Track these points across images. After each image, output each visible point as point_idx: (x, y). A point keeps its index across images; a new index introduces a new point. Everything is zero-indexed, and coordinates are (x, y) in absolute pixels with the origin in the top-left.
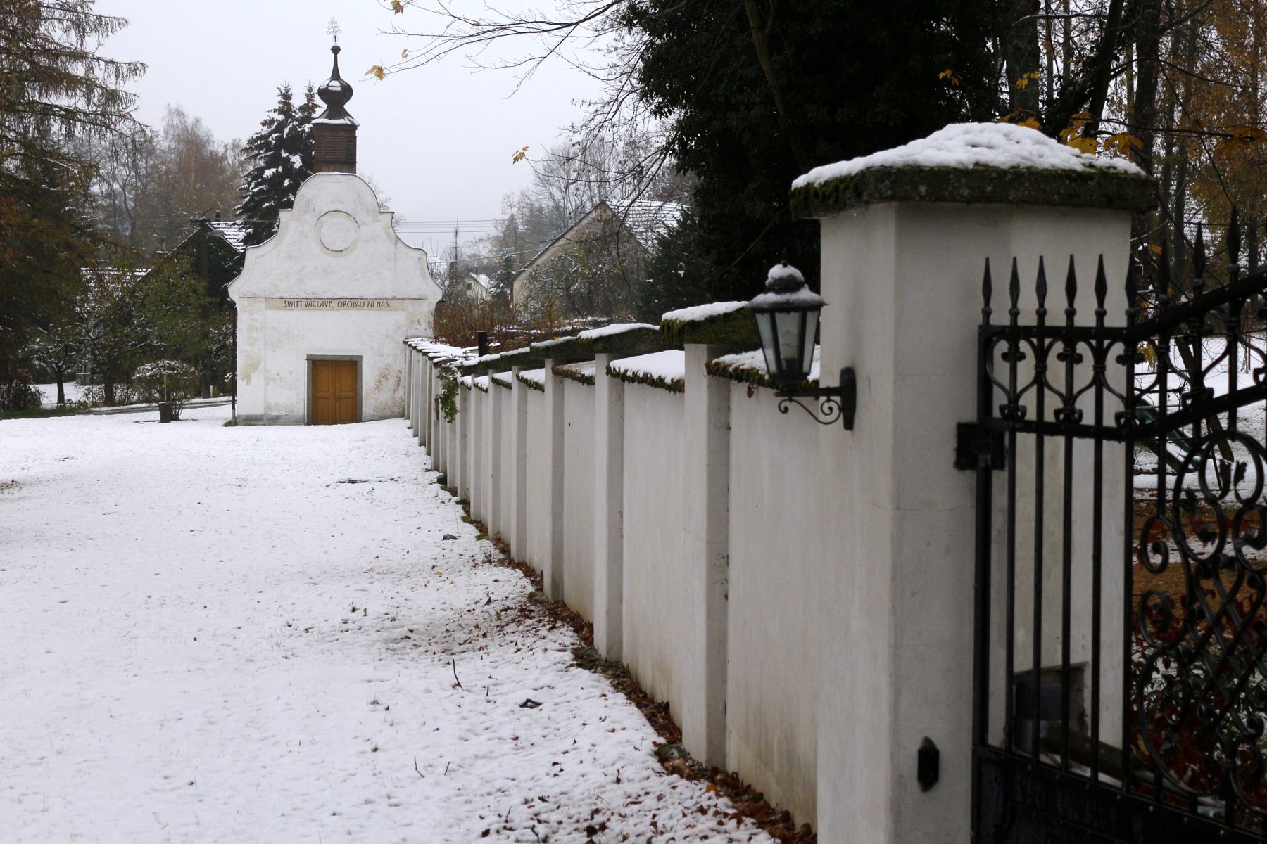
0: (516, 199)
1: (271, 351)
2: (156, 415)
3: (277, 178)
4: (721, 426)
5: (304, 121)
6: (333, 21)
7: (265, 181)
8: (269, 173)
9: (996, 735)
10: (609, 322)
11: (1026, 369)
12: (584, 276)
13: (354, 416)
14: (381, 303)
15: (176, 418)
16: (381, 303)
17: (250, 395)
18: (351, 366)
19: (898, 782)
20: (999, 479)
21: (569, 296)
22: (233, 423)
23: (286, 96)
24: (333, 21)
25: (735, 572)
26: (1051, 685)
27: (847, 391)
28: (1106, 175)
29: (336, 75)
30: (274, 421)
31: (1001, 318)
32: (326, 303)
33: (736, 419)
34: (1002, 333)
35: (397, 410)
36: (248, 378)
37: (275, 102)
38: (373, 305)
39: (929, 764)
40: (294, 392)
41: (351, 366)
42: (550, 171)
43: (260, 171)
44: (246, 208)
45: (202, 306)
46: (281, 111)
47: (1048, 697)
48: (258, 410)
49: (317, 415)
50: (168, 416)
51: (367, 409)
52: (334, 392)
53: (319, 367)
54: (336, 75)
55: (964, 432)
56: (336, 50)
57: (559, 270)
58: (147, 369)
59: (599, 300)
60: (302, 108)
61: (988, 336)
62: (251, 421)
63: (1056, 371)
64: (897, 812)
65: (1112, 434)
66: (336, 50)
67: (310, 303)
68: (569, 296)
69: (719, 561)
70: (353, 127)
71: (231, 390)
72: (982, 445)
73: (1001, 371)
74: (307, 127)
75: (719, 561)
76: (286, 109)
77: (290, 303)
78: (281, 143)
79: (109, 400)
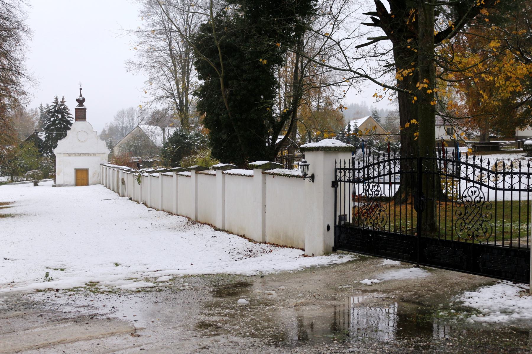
0: (109, 124)
1: (65, 168)
2: (33, 184)
3: (55, 121)
4: (264, 183)
5: (61, 105)
6: (80, 82)
7: (51, 121)
8: (52, 119)
9: (337, 224)
10: (281, 167)
11: (343, 174)
12: (135, 146)
13: (87, 184)
14: (94, 155)
15: (37, 185)
16: (94, 155)
17: (59, 179)
18: (86, 171)
19: (324, 230)
20: (338, 189)
21: (130, 151)
22: (53, 186)
23: (57, 99)
24: (80, 82)
25: (267, 208)
26: (343, 217)
27: (313, 177)
28: (350, 147)
29: (81, 96)
30: (66, 185)
31: (338, 167)
32: (79, 155)
33: (267, 182)
34: (338, 169)
35: (98, 182)
36: (59, 174)
37: (54, 100)
39: (328, 228)
40: (71, 178)
41: (86, 171)
42: (118, 116)
43: (50, 119)
44: (46, 129)
45: (37, 155)
46: (55, 103)
47: (343, 218)
48: (62, 183)
49: (77, 185)
50: (36, 185)
51: (90, 182)
52: (82, 178)
53: (77, 171)
54: (81, 96)
55: (333, 182)
56: (81, 89)
57: (127, 144)
58: (30, 172)
59: (138, 152)
60: (61, 102)
61: (336, 170)
62: (60, 185)
63: (347, 174)
64: (324, 234)
65: (347, 182)
66: (81, 89)
67: (75, 155)
68: (130, 151)
69: (264, 206)
70: (85, 109)
71: (54, 177)
72: (335, 184)
73: (338, 174)
74: (62, 107)
75: (264, 206)
76: (57, 102)
77: (70, 155)
78: (55, 111)
79: (12, 181)
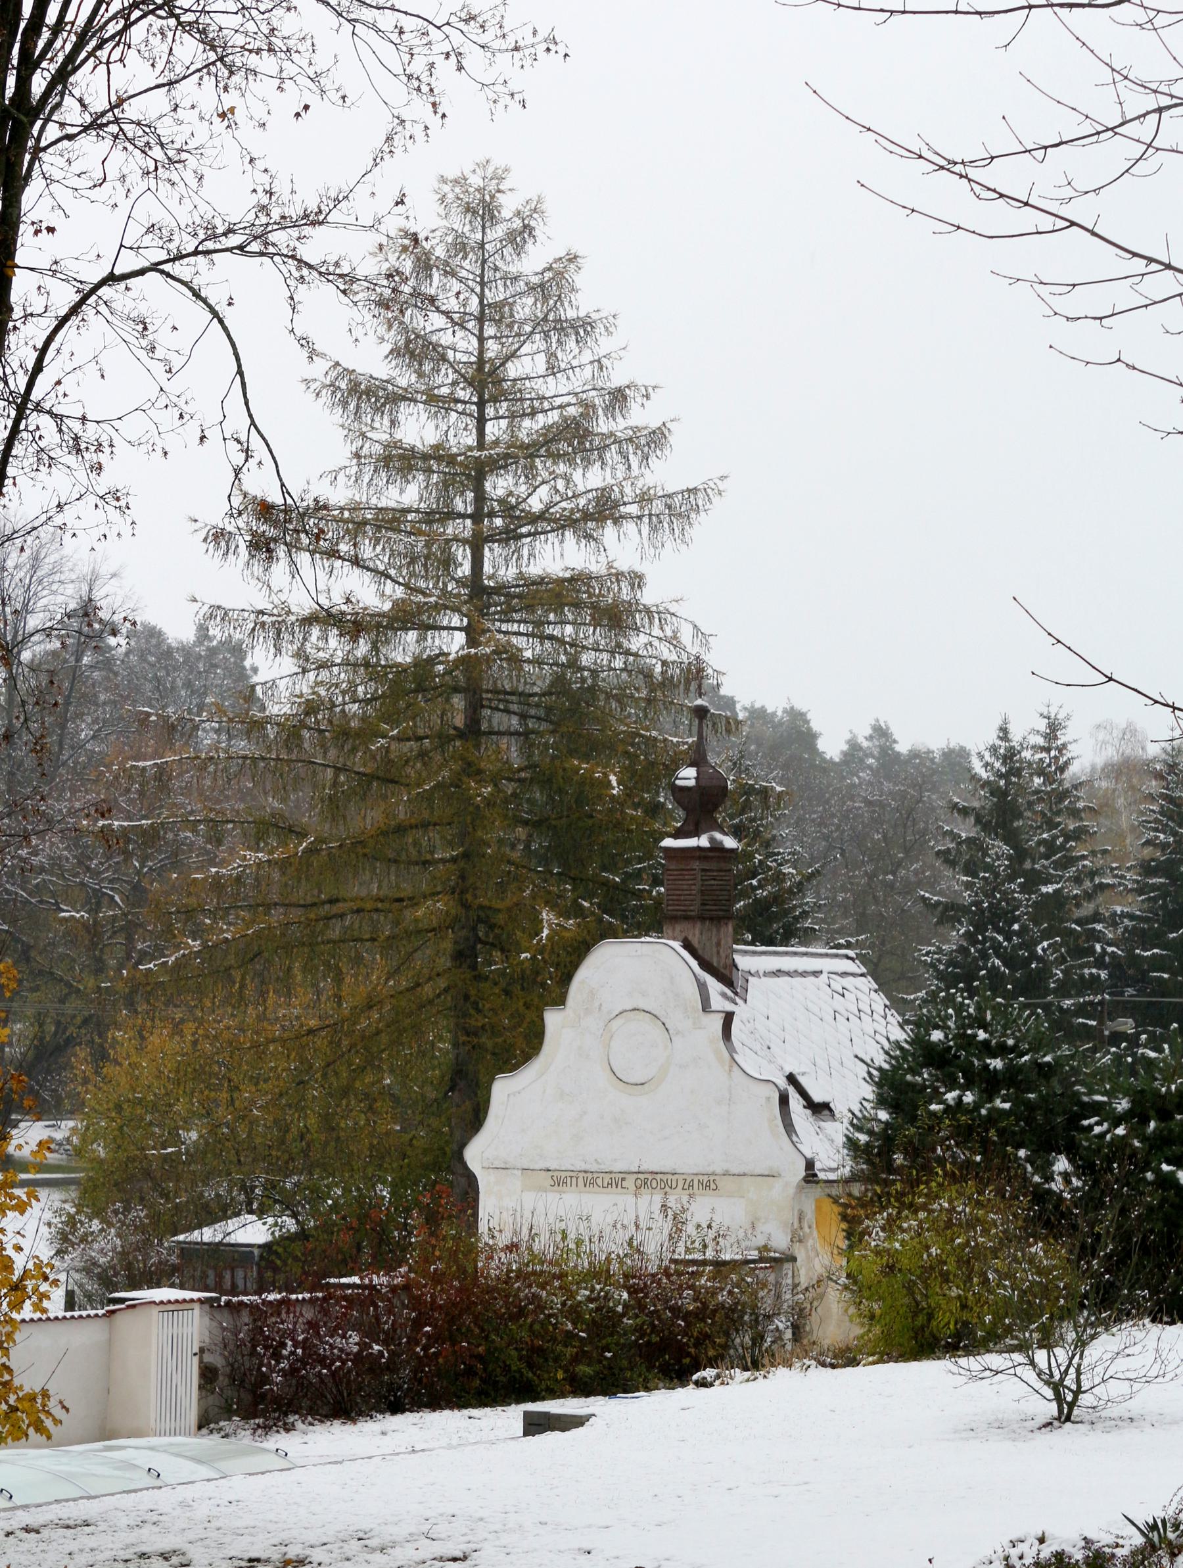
38: (593, 1183)
